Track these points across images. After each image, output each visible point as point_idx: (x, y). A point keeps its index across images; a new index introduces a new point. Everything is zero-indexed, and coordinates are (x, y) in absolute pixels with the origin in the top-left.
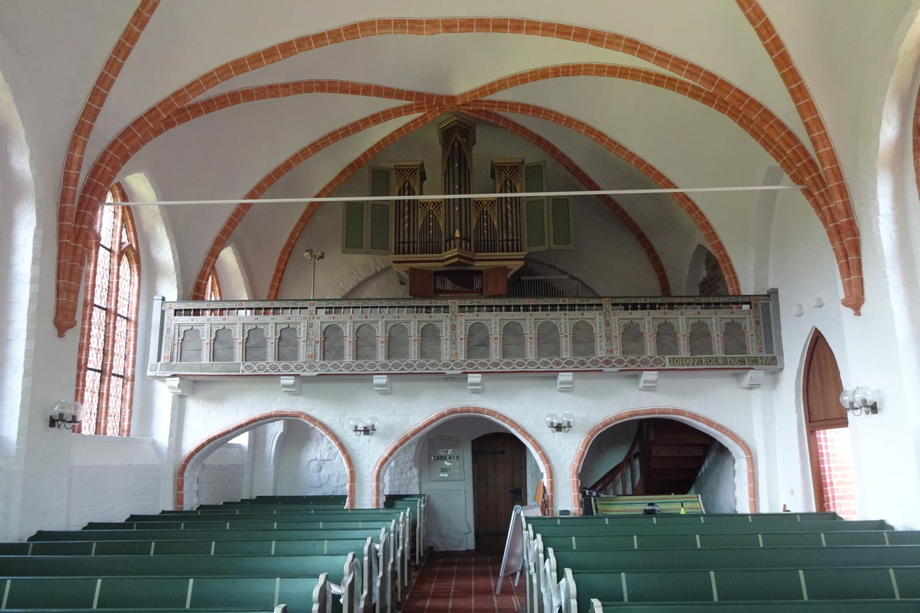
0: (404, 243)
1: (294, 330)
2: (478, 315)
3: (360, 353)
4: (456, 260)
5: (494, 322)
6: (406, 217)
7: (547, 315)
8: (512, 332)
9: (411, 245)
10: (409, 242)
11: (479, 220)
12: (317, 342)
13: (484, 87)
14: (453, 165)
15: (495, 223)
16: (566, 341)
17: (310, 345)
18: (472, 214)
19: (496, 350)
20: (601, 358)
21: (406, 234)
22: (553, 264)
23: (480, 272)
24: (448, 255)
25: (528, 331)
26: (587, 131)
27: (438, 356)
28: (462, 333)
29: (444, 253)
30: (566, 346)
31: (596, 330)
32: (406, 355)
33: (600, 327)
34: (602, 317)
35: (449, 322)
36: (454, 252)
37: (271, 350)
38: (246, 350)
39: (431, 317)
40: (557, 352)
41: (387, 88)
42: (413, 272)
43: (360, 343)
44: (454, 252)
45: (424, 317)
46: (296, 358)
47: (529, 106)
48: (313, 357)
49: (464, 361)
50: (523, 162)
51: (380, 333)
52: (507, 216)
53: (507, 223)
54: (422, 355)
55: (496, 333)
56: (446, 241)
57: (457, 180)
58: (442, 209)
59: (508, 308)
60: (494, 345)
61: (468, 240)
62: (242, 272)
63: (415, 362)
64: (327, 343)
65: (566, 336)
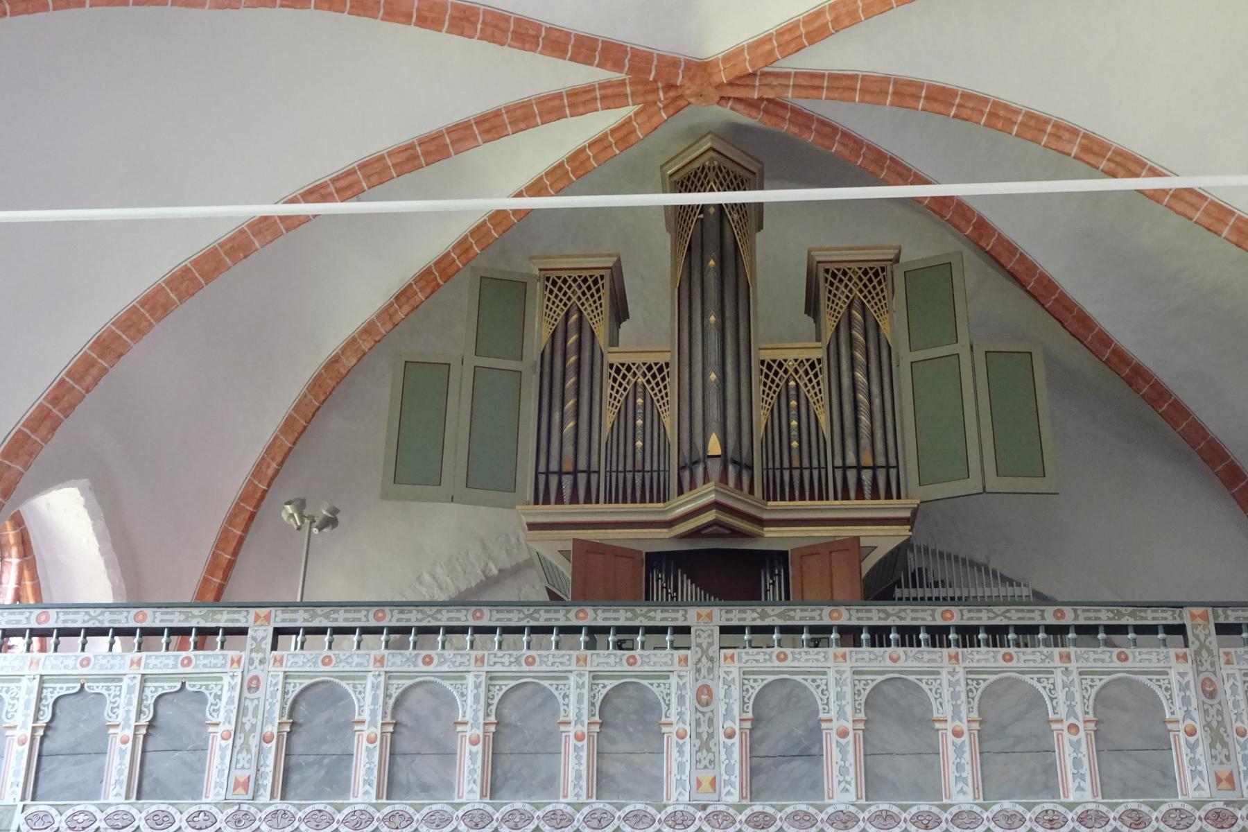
0: (560, 473)
1: (200, 697)
2: (782, 658)
3: (402, 777)
4: (710, 516)
5: (837, 680)
6: (570, 404)
7: (1008, 658)
8: (891, 708)
9: (582, 478)
10: (575, 472)
11: (776, 412)
12: (266, 739)
13: (792, 28)
14: (703, 263)
15: (824, 419)
16: (1076, 746)
17: (246, 747)
18: (757, 389)
19: (843, 771)
20: (1198, 804)
21: (569, 449)
22: (980, 558)
23: (779, 559)
24: (681, 505)
25: (948, 711)
26: (1085, 149)
27: (653, 788)
28: (731, 710)
29: (675, 501)
30: (1077, 763)
31: (1174, 710)
32: (550, 785)
33: (1186, 701)
34: (1182, 667)
35: (689, 677)
36: (706, 494)
37: (118, 763)
38: (39, 761)
39: (632, 661)
40: (1047, 781)
41: (520, 21)
42: (584, 554)
43: (405, 744)
44: (706, 494)
45: (608, 659)
46: (194, 789)
47: (918, 85)
48: (249, 786)
49: (740, 808)
50: (896, 260)
51: (471, 711)
52: (855, 403)
53: (857, 421)
54: (602, 782)
55: (841, 713)
56: (681, 469)
57: (714, 356)
58: (672, 382)
59: (879, 636)
60: (836, 755)
61: (745, 466)
62: (107, 563)
63: (578, 807)
64: (299, 741)
65: (1073, 728)
